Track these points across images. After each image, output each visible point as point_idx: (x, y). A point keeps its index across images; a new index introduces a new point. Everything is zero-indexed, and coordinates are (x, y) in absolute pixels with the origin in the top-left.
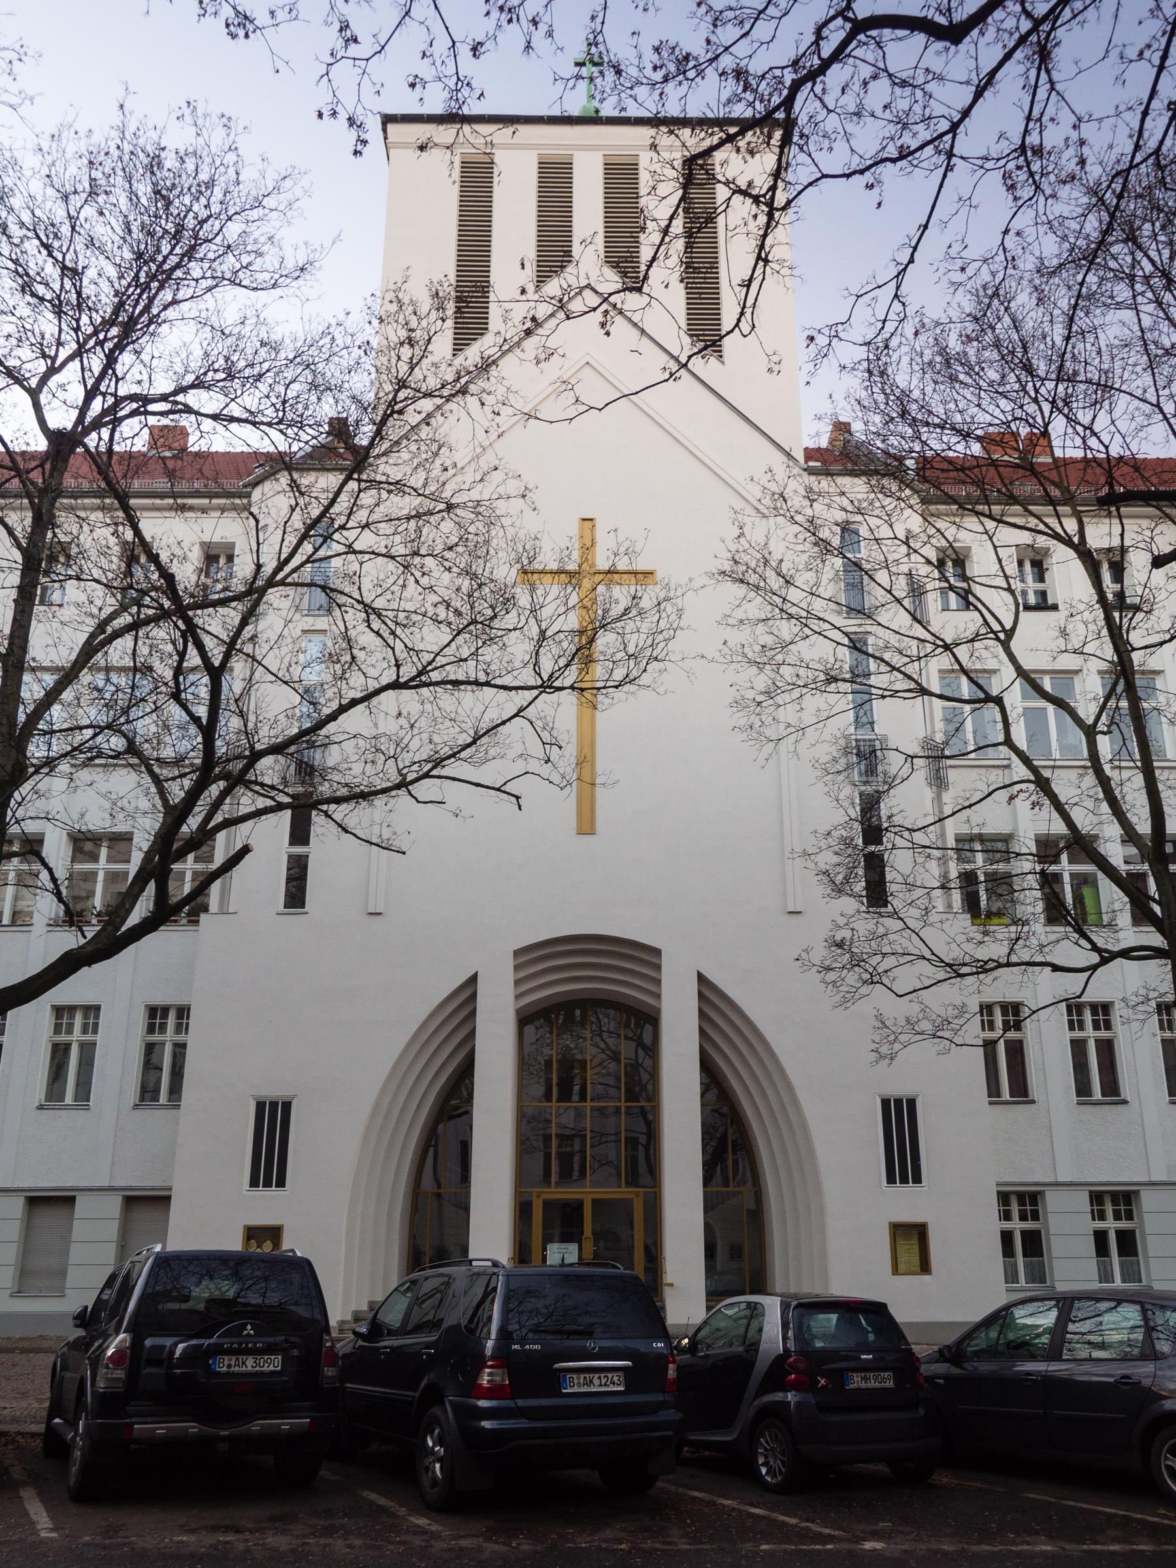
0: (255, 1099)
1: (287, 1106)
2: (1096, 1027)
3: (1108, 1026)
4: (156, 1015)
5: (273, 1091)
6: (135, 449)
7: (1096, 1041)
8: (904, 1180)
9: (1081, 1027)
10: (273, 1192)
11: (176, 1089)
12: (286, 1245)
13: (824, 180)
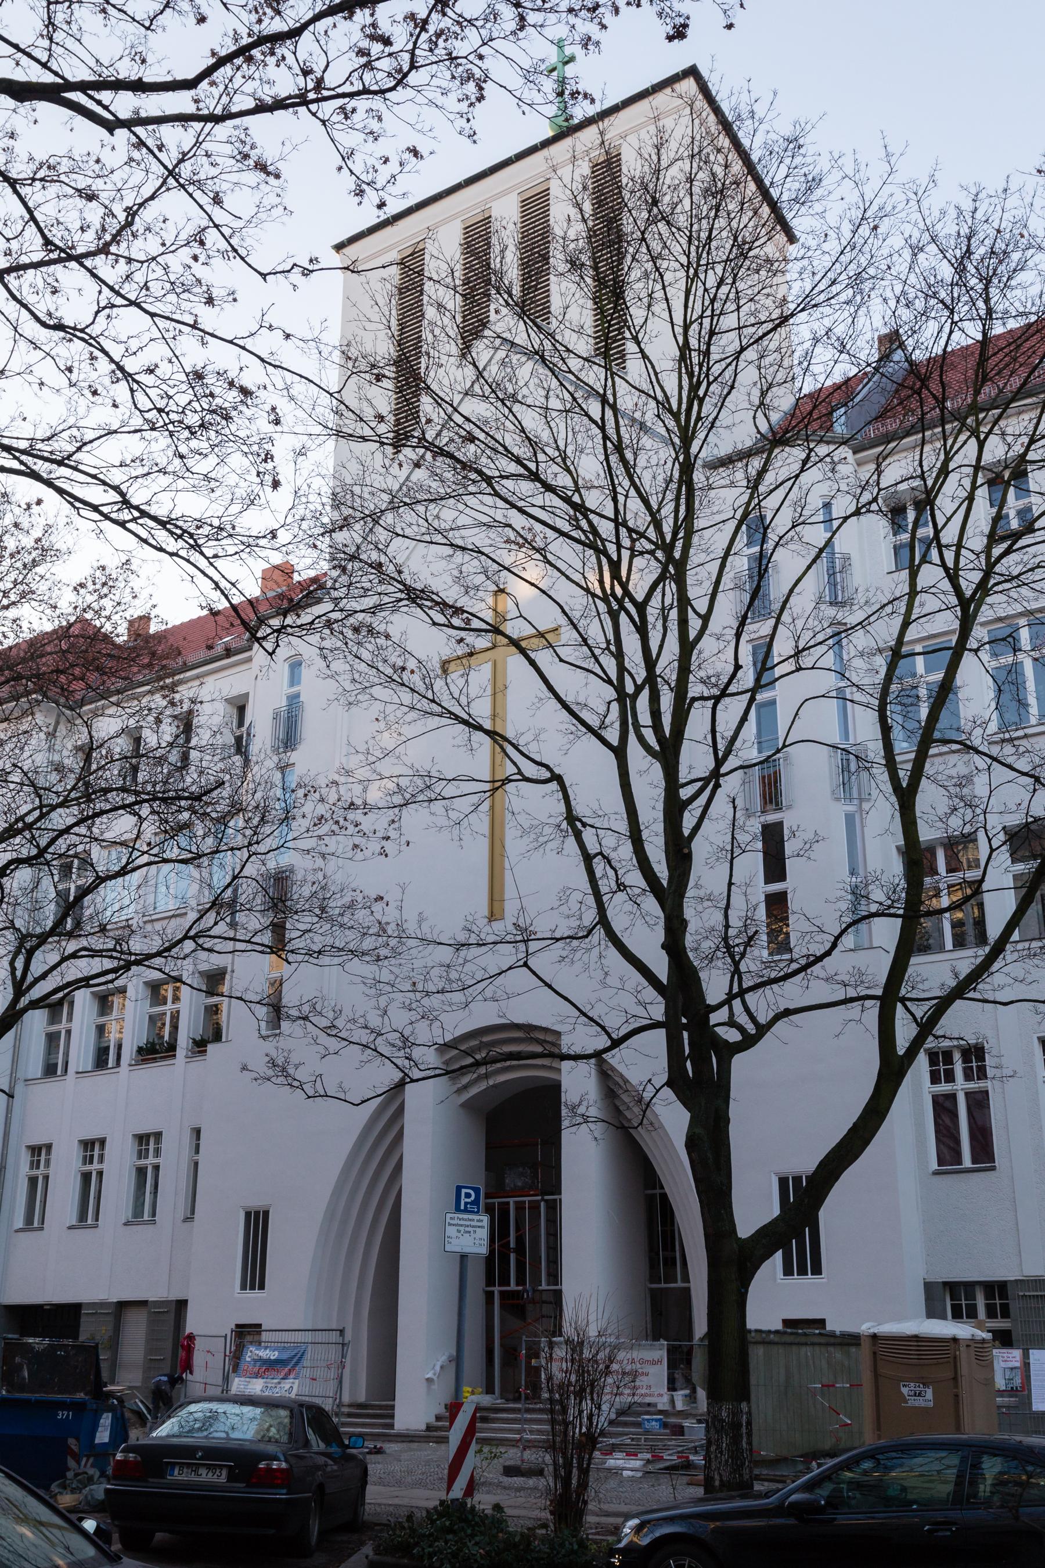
0: (243, 1208)
1: (266, 1213)
2: (968, 1077)
3: (982, 1074)
4: (141, 1139)
5: (256, 1203)
6: (428, 286)
7: (966, 1094)
8: (802, 1272)
9: (950, 1077)
10: (256, 1294)
11: (42, 1221)
12: (829, 1327)
13: (190, 75)
